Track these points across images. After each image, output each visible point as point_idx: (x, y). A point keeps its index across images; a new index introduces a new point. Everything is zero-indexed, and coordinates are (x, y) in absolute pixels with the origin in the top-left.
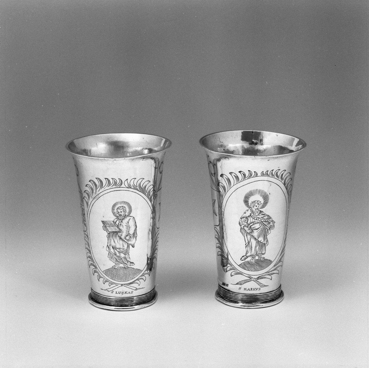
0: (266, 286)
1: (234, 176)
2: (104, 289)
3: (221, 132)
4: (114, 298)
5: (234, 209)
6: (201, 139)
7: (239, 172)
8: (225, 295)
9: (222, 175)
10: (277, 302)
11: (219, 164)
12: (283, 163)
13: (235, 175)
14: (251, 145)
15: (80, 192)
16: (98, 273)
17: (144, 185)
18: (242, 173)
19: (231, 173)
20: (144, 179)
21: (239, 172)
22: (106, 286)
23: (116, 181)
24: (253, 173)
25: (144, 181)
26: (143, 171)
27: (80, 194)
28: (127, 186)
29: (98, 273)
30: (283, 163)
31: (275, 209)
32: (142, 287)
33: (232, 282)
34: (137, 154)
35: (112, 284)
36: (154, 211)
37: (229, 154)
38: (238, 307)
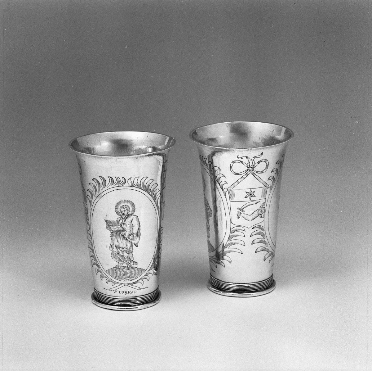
15: (84, 190)
27: (83, 194)
32: (147, 286)
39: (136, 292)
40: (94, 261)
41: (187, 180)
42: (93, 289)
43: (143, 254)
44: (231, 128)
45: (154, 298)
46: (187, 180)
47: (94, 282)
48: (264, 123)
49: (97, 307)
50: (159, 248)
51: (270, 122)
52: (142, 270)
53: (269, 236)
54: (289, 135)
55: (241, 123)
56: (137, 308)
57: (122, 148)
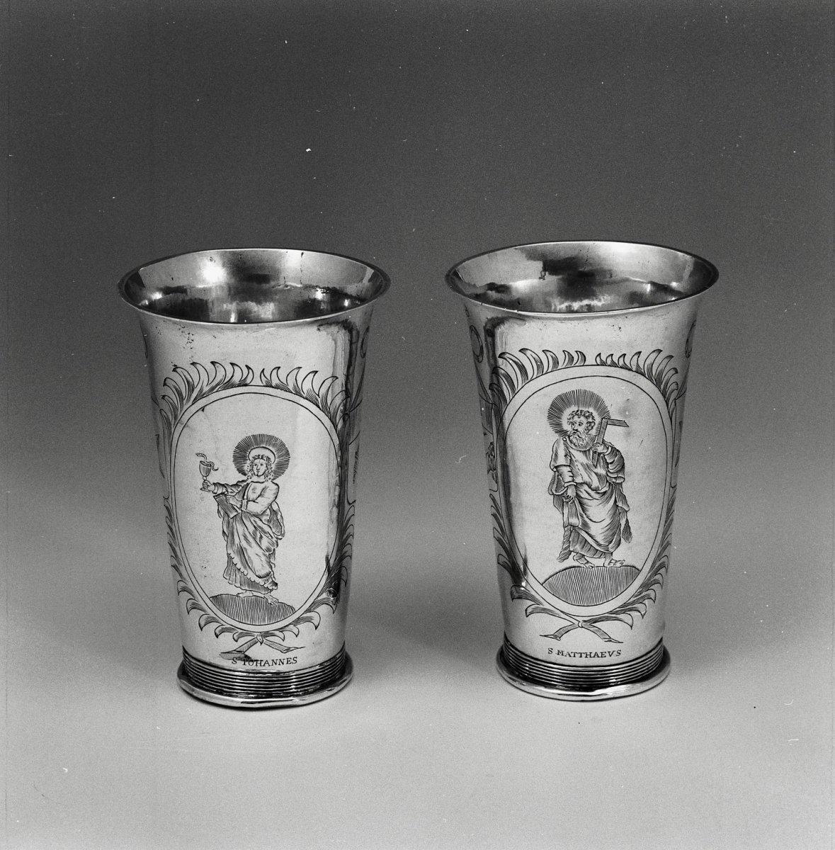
0: (619, 642)
1: (552, 357)
2: (213, 648)
3: (468, 259)
4: (245, 674)
5: (532, 440)
6: (715, 282)
7: (520, 351)
8: (519, 667)
9: (502, 356)
10: (647, 685)
11: (499, 331)
12: (646, 333)
13: (534, 355)
14: (245, 283)
15: (154, 400)
16: (202, 610)
17: (649, 362)
18: (528, 353)
19: (522, 350)
20: (279, 368)
21: (520, 351)
22: (227, 642)
23: (191, 380)
24: (561, 357)
25: (643, 357)
26: (312, 351)
27: (159, 409)
28: (265, 384)
29: (202, 610)
30: (646, 333)
31: (639, 442)
32: (307, 647)
33: (537, 636)
34: (304, 309)
35: (241, 635)
36: (343, 448)
37: (519, 307)
38: (552, 697)
39: (297, 660)
40: (182, 584)
41: (418, 385)
42: (182, 651)
43: (300, 566)
44: (223, 266)
45: (334, 674)
46: (418, 385)
47: (184, 631)
48: (642, 245)
49: (513, 688)
50: (665, 545)
51: (663, 244)
52: (287, 609)
53: (235, 537)
54: (705, 275)
55: (244, 252)
56: (291, 700)
57: (579, 280)
